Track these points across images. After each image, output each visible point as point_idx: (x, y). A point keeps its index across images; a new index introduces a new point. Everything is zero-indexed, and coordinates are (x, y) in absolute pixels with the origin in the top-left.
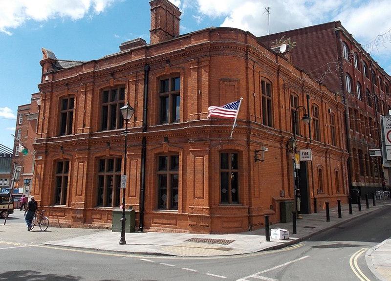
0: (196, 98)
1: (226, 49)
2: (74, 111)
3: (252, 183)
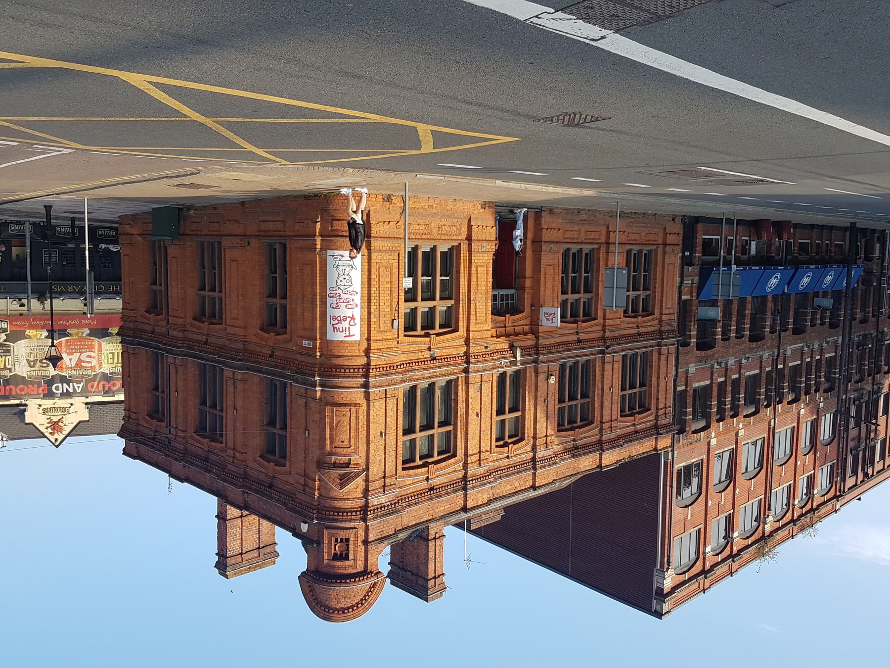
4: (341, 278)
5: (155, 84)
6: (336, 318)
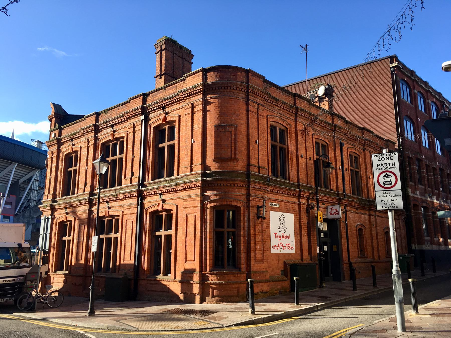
1: (221, 90)
3: (252, 244)
4: (283, 221)
5: (380, 288)
6: (336, 214)
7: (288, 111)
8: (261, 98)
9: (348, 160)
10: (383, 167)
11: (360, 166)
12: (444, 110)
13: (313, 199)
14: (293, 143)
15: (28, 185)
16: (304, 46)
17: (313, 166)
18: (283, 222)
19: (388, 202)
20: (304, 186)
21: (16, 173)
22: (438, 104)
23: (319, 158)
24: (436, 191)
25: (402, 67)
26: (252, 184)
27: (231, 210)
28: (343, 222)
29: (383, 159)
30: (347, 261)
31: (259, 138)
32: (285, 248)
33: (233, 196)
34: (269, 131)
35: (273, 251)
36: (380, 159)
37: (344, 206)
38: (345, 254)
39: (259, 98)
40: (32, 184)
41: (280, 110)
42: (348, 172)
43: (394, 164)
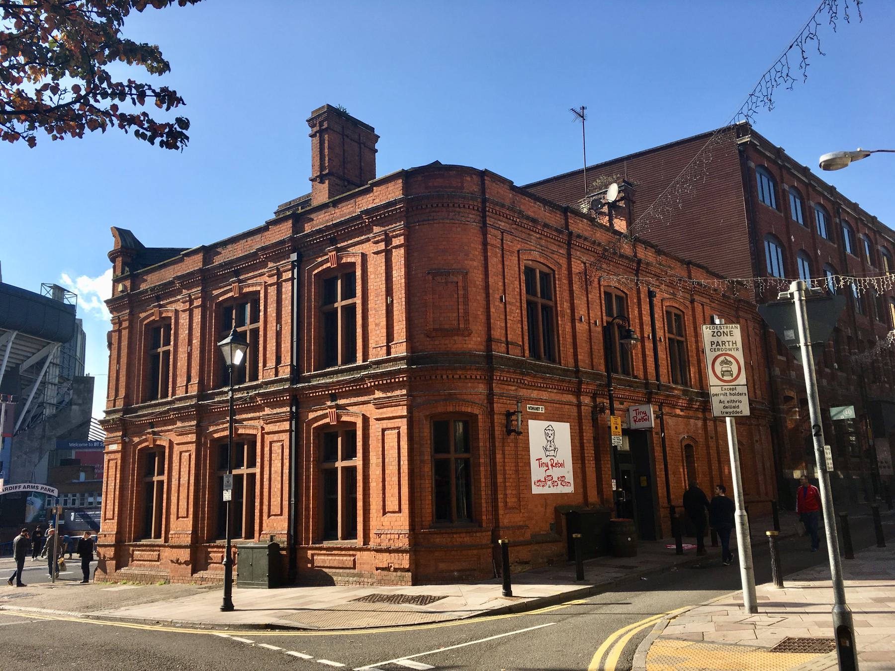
0: (384, 312)
1: (437, 209)
2: (172, 349)
3: (500, 479)
4: (552, 437)
6: (645, 420)
7: (555, 239)
8: (506, 220)
9: (663, 321)
10: (720, 348)
11: (686, 331)
12: (839, 218)
13: (603, 396)
14: (565, 297)
15: (38, 375)
16: (578, 110)
17: (601, 337)
18: (551, 439)
19: (729, 404)
20: (586, 373)
21: (13, 351)
22: (829, 207)
23: (613, 320)
24: (828, 370)
25: (758, 144)
26: (496, 374)
27: (460, 421)
28: (657, 433)
29: (719, 334)
30: (666, 505)
31: (506, 292)
32: (556, 484)
33: (465, 397)
34: (523, 277)
35: (536, 490)
36: (715, 334)
37: (659, 405)
38: (661, 491)
39: (504, 219)
40: (46, 372)
41: (540, 238)
42: (663, 343)
43: (736, 343)
